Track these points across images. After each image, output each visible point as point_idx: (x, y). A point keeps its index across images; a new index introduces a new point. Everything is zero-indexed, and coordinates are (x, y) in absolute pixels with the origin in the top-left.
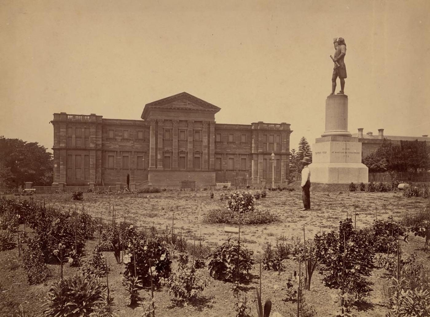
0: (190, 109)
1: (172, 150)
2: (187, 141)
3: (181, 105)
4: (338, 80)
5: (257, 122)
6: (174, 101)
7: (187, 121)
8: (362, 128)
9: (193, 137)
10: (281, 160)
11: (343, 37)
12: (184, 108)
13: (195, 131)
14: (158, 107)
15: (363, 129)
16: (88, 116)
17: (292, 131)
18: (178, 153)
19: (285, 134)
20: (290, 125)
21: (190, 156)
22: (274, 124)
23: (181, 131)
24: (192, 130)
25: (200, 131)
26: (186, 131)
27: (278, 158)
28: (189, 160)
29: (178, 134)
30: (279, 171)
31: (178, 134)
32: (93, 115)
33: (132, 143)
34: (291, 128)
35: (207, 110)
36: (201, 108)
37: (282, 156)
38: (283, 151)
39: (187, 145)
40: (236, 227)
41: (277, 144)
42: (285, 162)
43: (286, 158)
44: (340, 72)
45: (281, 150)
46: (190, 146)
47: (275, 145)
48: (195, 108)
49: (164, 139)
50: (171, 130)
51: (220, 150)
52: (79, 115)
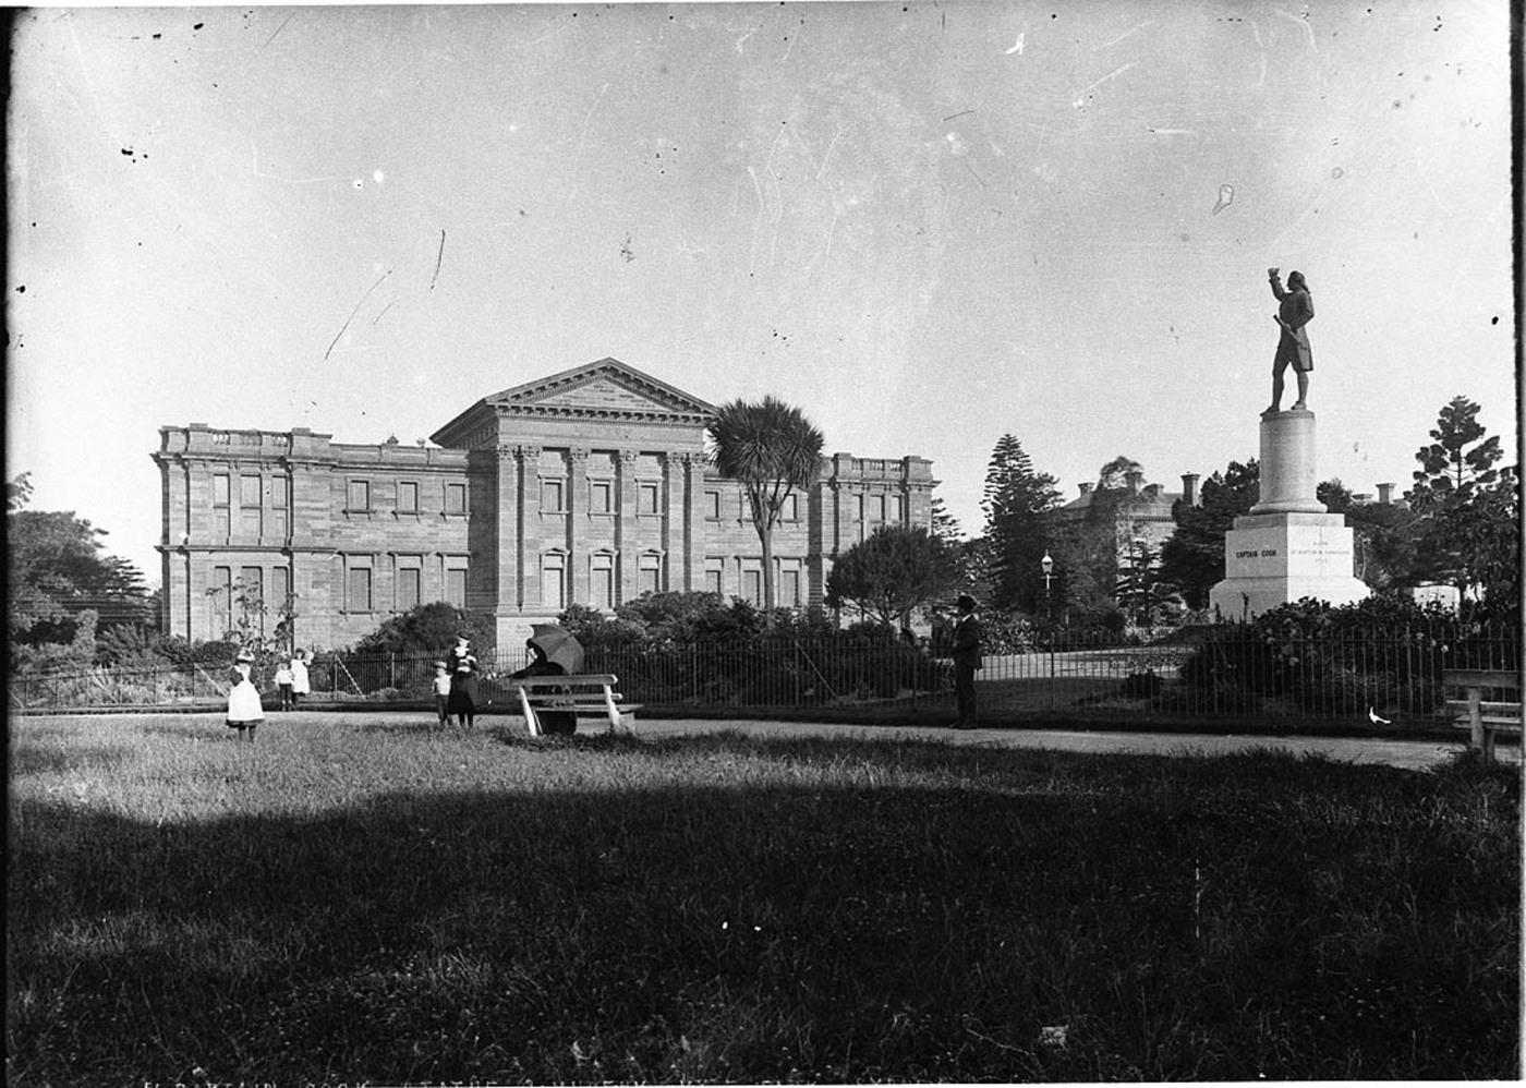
4: (1290, 375)
8: (151, 459)
11: (1414, 457)
15: (152, 455)
17: (939, 482)
33: (430, 526)
35: (680, 415)
36: (547, 402)
40: (1361, 497)
44: (1292, 353)
51: (716, 545)
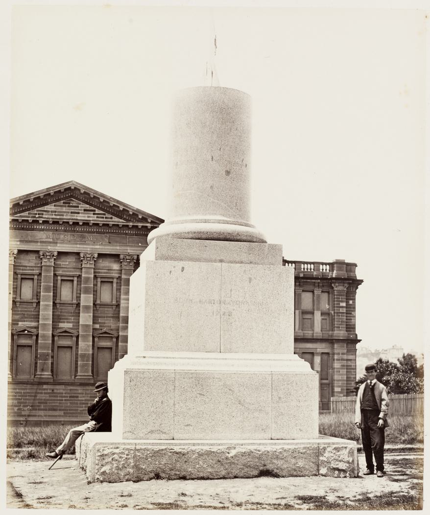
0: (86, 224)
1: (37, 328)
2: (78, 305)
3: (66, 213)
5: (332, 262)
6: (47, 204)
7: (78, 254)
9: (95, 295)
10: (334, 354)
12: (51, 221)
13: (99, 280)
14: (142, 225)
16: (326, 264)
18: (53, 336)
19: (341, 288)
20: (355, 265)
21: (85, 346)
22: (313, 263)
23: (101, 282)
24: (92, 276)
25: (115, 280)
26: (75, 279)
27: (326, 351)
28: (83, 356)
29: (55, 287)
30: (329, 384)
31: (55, 287)
32: (336, 260)
34: (359, 274)
37: (336, 346)
38: (341, 333)
39: (78, 315)
41: (322, 314)
42: (343, 360)
43: (345, 351)
45: (333, 330)
46: (86, 318)
47: (318, 317)
48: (101, 221)
49: (57, 301)
50: (36, 277)
52: (307, 263)
